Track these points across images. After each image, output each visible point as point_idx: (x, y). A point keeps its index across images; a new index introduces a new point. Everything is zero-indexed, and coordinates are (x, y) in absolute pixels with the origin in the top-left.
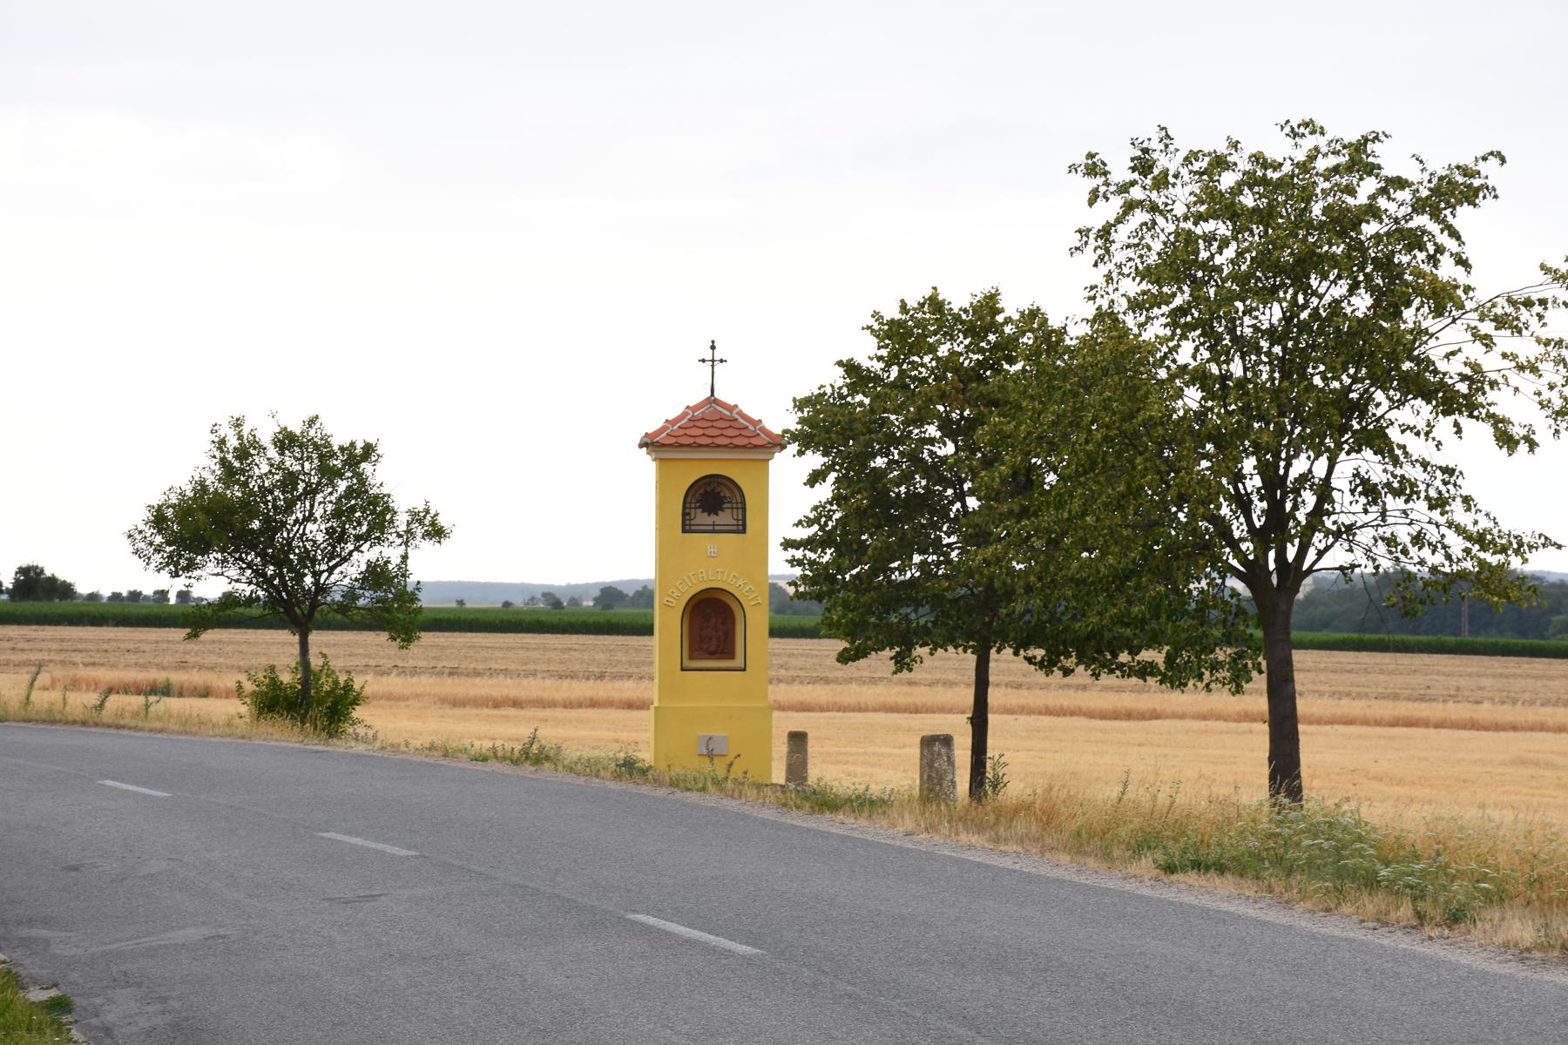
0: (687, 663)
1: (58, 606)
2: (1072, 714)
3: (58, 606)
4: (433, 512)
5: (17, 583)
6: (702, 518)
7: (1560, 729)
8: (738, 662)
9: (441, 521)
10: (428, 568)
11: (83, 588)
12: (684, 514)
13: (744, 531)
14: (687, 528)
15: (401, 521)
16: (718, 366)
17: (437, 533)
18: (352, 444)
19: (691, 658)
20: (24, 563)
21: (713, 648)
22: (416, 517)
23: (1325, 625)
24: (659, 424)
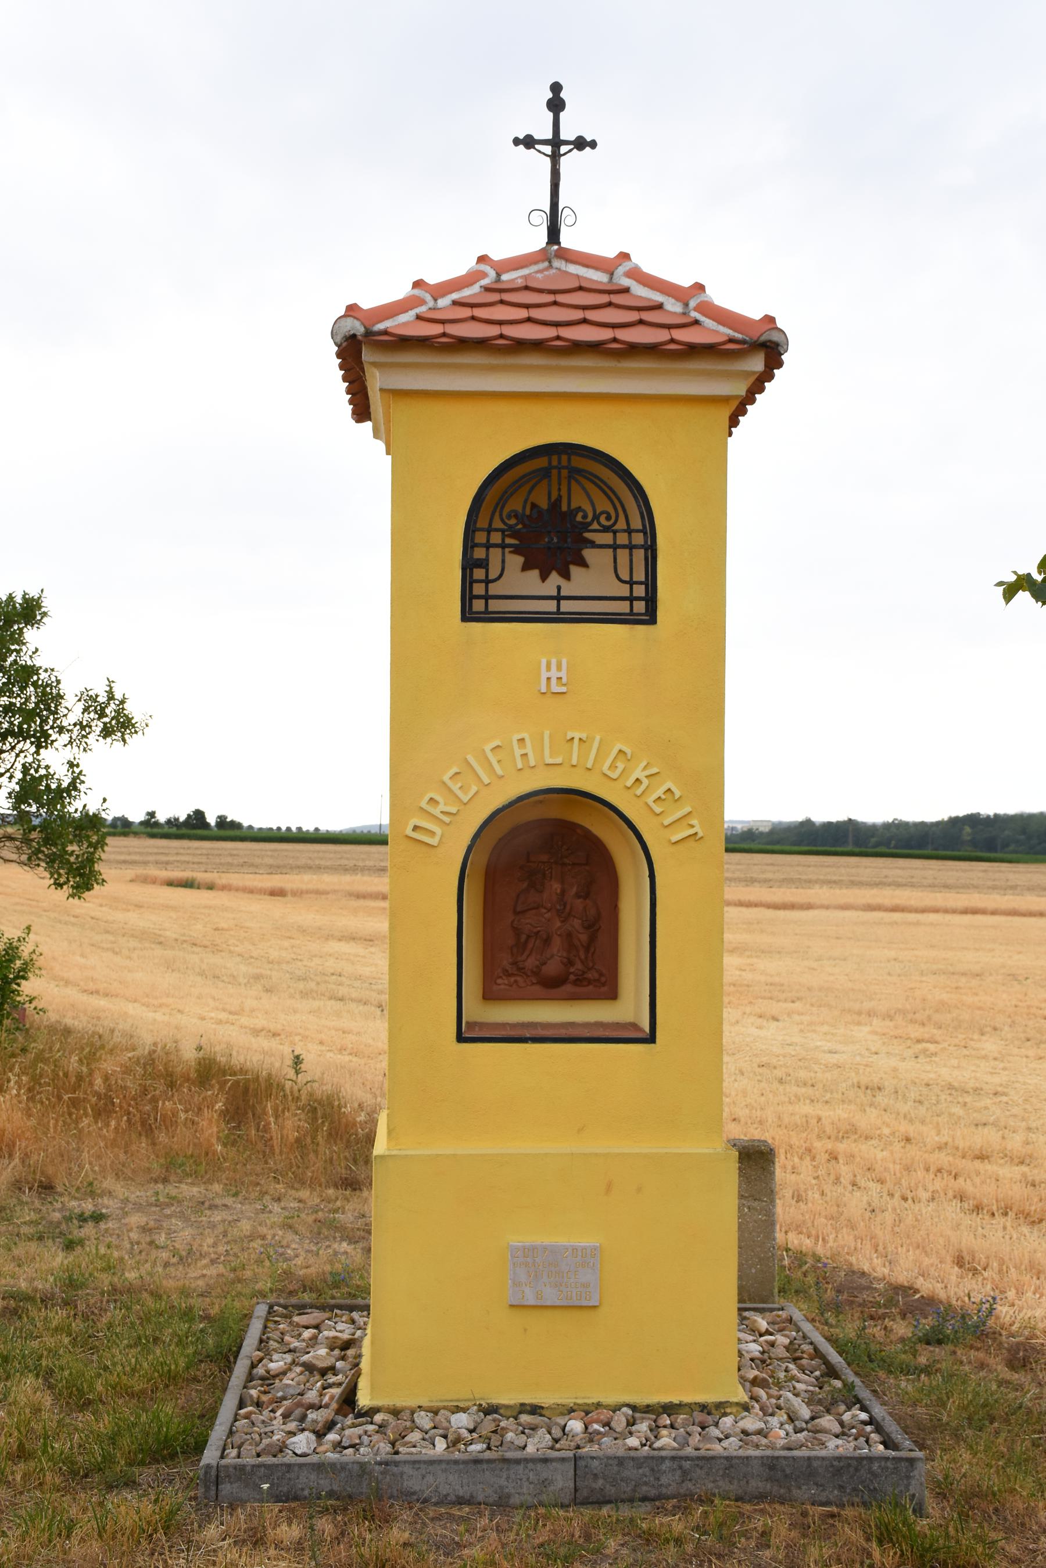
0: (477, 1011)
1: (236, 833)
2: (756, 905)
3: (236, 833)
4: (118, 696)
5: (217, 823)
6: (517, 580)
7: (1041, 914)
8: (629, 1007)
9: (130, 708)
10: (113, 782)
11: (245, 824)
12: (469, 565)
13: (650, 617)
14: (476, 606)
15: (72, 711)
16: (571, 161)
17: (119, 726)
18: (11, 597)
19: (489, 995)
20: (220, 814)
21: (553, 968)
22: (92, 704)
23: (778, 842)
24: (400, 290)
